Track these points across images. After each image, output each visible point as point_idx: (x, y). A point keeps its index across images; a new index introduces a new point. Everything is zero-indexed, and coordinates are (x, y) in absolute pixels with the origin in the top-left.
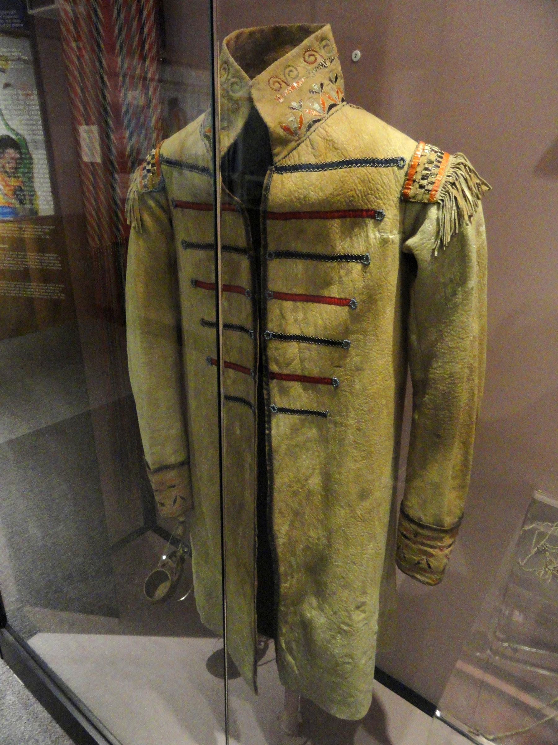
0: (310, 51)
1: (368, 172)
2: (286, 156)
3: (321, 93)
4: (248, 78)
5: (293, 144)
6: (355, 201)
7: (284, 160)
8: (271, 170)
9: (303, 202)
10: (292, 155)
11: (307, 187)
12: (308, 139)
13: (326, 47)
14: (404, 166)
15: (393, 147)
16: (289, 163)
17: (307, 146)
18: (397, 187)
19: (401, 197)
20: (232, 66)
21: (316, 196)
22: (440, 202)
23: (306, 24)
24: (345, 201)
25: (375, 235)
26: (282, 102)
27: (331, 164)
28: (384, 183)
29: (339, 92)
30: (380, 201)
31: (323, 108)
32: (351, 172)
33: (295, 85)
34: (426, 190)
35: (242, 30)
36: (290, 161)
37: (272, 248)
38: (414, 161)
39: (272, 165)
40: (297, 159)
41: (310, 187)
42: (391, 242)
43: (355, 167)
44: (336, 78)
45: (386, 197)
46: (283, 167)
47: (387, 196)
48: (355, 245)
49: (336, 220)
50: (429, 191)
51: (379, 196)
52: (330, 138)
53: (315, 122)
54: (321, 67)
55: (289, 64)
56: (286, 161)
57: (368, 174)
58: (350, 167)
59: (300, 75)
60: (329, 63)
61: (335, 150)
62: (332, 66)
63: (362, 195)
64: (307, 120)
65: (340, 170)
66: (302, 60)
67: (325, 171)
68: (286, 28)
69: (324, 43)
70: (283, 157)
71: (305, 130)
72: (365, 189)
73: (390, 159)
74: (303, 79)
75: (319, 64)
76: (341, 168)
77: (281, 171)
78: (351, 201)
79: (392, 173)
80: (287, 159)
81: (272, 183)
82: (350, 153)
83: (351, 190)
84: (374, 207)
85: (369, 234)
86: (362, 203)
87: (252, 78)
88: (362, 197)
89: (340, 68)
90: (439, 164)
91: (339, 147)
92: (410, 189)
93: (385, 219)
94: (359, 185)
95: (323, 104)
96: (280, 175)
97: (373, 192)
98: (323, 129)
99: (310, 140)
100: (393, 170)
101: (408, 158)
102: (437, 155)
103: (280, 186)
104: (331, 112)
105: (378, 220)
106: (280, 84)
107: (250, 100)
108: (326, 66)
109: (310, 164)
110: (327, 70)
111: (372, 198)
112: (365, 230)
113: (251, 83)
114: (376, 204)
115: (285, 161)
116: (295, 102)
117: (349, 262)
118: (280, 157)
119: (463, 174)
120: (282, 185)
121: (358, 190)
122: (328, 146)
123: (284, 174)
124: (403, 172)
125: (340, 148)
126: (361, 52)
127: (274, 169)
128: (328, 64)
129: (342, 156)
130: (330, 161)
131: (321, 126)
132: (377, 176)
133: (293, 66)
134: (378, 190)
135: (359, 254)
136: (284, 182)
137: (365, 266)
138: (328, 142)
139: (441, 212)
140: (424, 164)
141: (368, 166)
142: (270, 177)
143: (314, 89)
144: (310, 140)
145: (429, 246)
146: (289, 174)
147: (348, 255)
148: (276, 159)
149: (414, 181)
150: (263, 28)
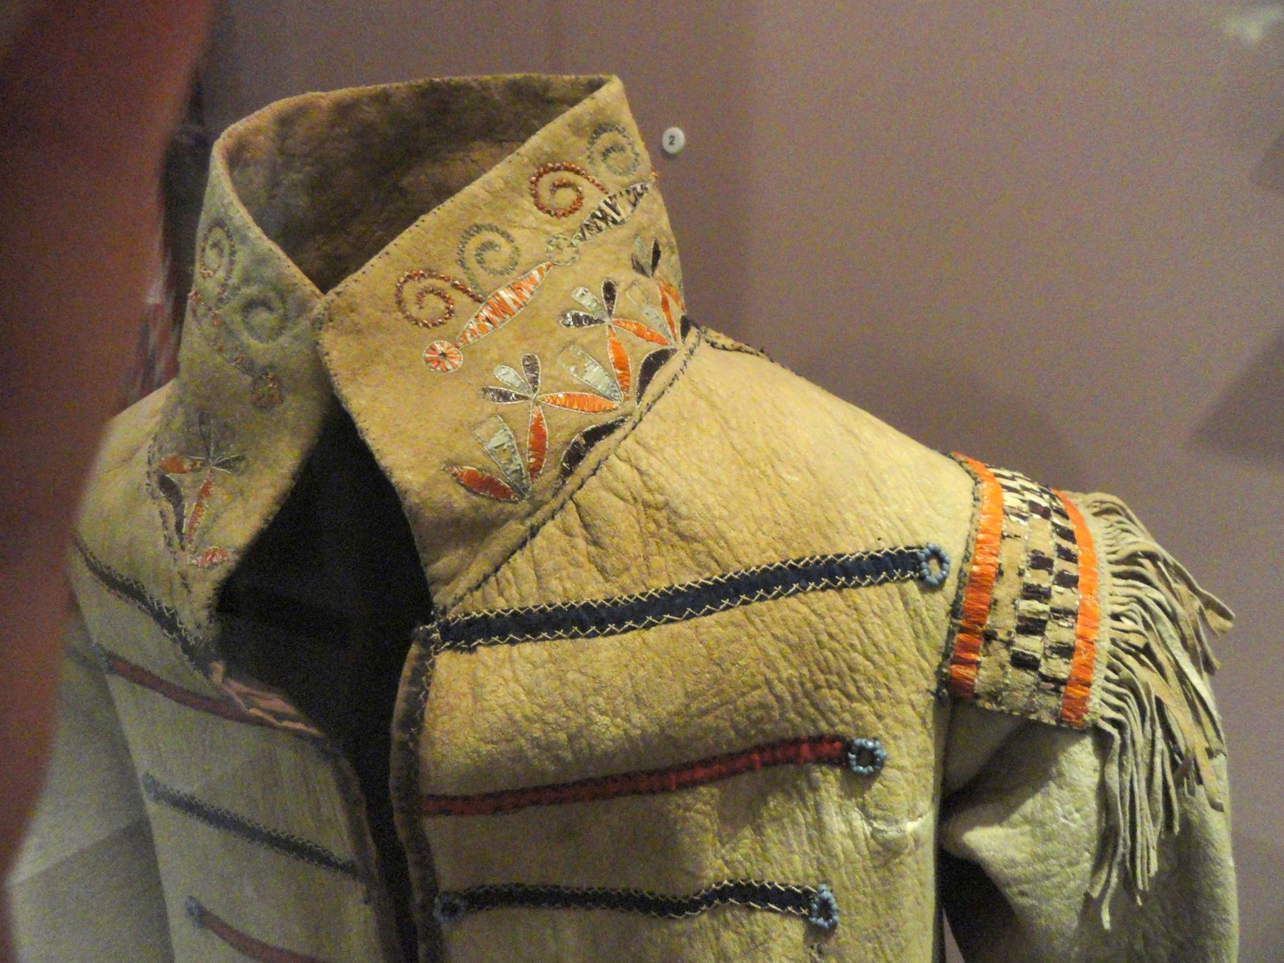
0: (554, 170)
1: (814, 611)
2: (486, 578)
3: (607, 320)
4: (308, 286)
5: (515, 529)
6: (771, 720)
7: (478, 594)
8: (426, 642)
9: (568, 756)
10: (509, 575)
11: (579, 699)
12: (570, 505)
13: (613, 155)
14: (942, 582)
15: (895, 507)
16: (501, 604)
17: (568, 533)
18: (923, 656)
19: (938, 690)
20: (244, 240)
21: (618, 727)
22: (1108, 728)
23: (535, 75)
24: (734, 726)
25: (849, 823)
26: (460, 371)
27: (671, 598)
28: (876, 646)
29: (671, 302)
30: (864, 708)
31: (620, 377)
32: (752, 623)
33: (506, 295)
34: (1044, 678)
35: (310, 95)
36: (501, 594)
37: (449, 875)
38: (979, 558)
39: (428, 620)
40: (529, 587)
41: (590, 700)
42: (911, 842)
43: (762, 599)
44: (656, 254)
45: (884, 692)
46: (472, 623)
47: (889, 689)
48: (775, 852)
49: (703, 790)
50: (1059, 682)
51: (858, 688)
52: (660, 498)
53: (594, 436)
54: (601, 224)
55: (478, 221)
56: (484, 599)
57: (814, 618)
58: (745, 603)
59: (522, 260)
60: (629, 208)
61: (683, 544)
62: (640, 217)
63: (793, 695)
64: (562, 436)
65: (707, 620)
66: (528, 203)
67: (647, 627)
68: (464, 89)
69: (606, 139)
70: (474, 583)
71: (556, 472)
72: (805, 671)
73: (887, 554)
74: (535, 273)
75: (594, 216)
76: (710, 612)
77: (469, 642)
78: (755, 723)
79: (900, 605)
80: (491, 589)
81: (432, 695)
82: (740, 551)
83: (757, 687)
84: (840, 728)
85: (826, 819)
86: (798, 720)
87: (325, 282)
88: (795, 700)
89: (665, 221)
90: (1071, 569)
91: (697, 528)
92: (978, 664)
93: (888, 772)
94: (782, 664)
95: (621, 364)
96: (465, 656)
97: (835, 679)
98: (628, 461)
99: (578, 506)
100: (903, 595)
101: (954, 551)
102: (1054, 524)
103: (467, 702)
104: (652, 389)
105: (860, 774)
106: (447, 300)
107: (322, 380)
108: (618, 218)
109: (587, 607)
110: (621, 233)
111: (832, 699)
112: (811, 803)
113: (320, 304)
114: (847, 717)
115: (484, 599)
116: (511, 366)
117: (752, 909)
118: (461, 586)
119: (1161, 598)
120: (476, 699)
121: (780, 681)
122: (652, 526)
123: (482, 650)
124: (941, 602)
125: (702, 534)
126: (684, 131)
127: (436, 635)
128: (625, 210)
129: (714, 565)
130: (663, 586)
131: (621, 451)
132: (848, 622)
133: (491, 228)
134: (852, 669)
135: (792, 884)
136: (482, 686)
137: (819, 935)
138: (650, 511)
139: (1113, 769)
140: (1021, 574)
141: (814, 589)
142: (423, 674)
143: (582, 308)
144: (578, 506)
145: (1072, 885)
146: (503, 650)
147: (750, 885)
148: (441, 597)
149: (989, 637)
150: (385, 88)
